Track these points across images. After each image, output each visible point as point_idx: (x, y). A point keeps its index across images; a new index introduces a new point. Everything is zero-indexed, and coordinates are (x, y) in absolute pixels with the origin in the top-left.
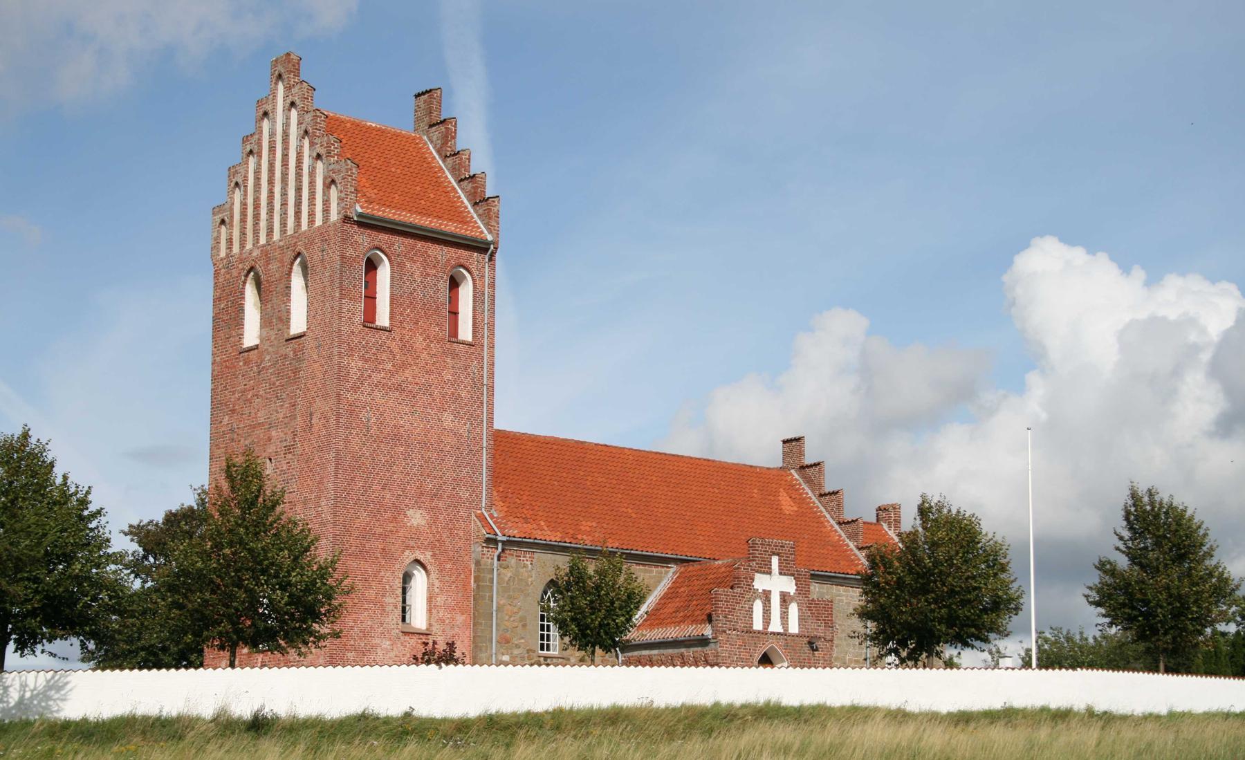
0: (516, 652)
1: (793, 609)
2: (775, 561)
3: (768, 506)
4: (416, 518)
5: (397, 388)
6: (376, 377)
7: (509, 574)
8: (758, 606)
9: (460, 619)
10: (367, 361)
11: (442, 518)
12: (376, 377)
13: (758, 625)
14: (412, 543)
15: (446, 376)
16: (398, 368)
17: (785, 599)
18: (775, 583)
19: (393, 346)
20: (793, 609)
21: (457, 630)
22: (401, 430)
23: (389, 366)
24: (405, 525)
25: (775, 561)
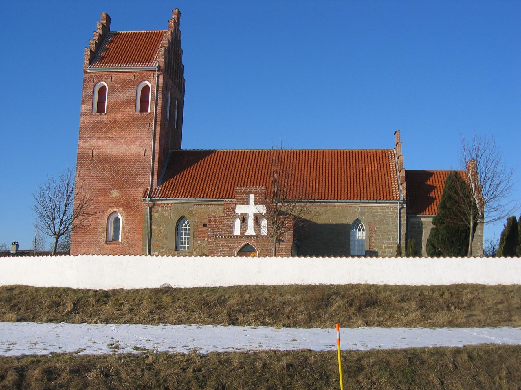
0: (162, 250)
1: (264, 223)
2: (252, 197)
3: (357, 173)
4: (115, 193)
5: (108, 138)
6: (97, 135)
7: (158, 215)
8: (238, 223)
9: (137, 236)
10: (93, 129)
11: (128, 192)
12: (97, 135)
13: (237, 231)
14: (112, 205)
15: (134, 129)
16: (108, 130)
17: (257, 219)
18: (251, 208)
19: (106, 121)
20: (264, 223)
21: (135, 242)
22: (109, 156)
23: (104, 130)
24: (109, 197)
25: (252, 197)
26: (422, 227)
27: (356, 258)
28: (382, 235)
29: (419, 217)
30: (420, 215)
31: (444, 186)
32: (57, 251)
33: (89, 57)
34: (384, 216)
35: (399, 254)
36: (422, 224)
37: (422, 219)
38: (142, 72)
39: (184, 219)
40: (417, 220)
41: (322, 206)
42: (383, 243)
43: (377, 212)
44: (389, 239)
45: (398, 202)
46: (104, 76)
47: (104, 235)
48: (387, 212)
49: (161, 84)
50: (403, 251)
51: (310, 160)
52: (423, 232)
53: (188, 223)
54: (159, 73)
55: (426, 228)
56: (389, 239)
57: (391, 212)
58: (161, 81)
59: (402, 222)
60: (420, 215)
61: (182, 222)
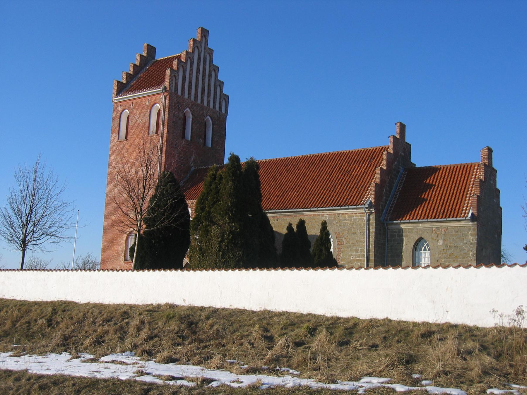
26: (402, 236)
27: (62, 271)
28: (350, 247)
29: (397, 223)
30: (399, 221)
31: (163, 170)
32: (24, 268)
33: (116, 88)
34: (352, 224)
35: (368, 267)
36: (403, 232)
37: (401, 226)
38: (154, 95)
39: (422, 241)
40: (397, 226)
41: (291, 216)
42: (351, 256)
43: (345, 220)
44: (357, 251)
45: (363, 206)
46: (127, 104)
47: (123, 254)
48: (355, 220)
49: (167, 105)
50: (372, 263)
51: (463, 176)
52: (404, 242)
53: (427, 245)
54: (166, 94)
55: (407, 236)
56: (357, 251)
57: (359, 219)
58: (167, 102)
59: (371, 230)
60: (399, 221)
61: (420, 244)
